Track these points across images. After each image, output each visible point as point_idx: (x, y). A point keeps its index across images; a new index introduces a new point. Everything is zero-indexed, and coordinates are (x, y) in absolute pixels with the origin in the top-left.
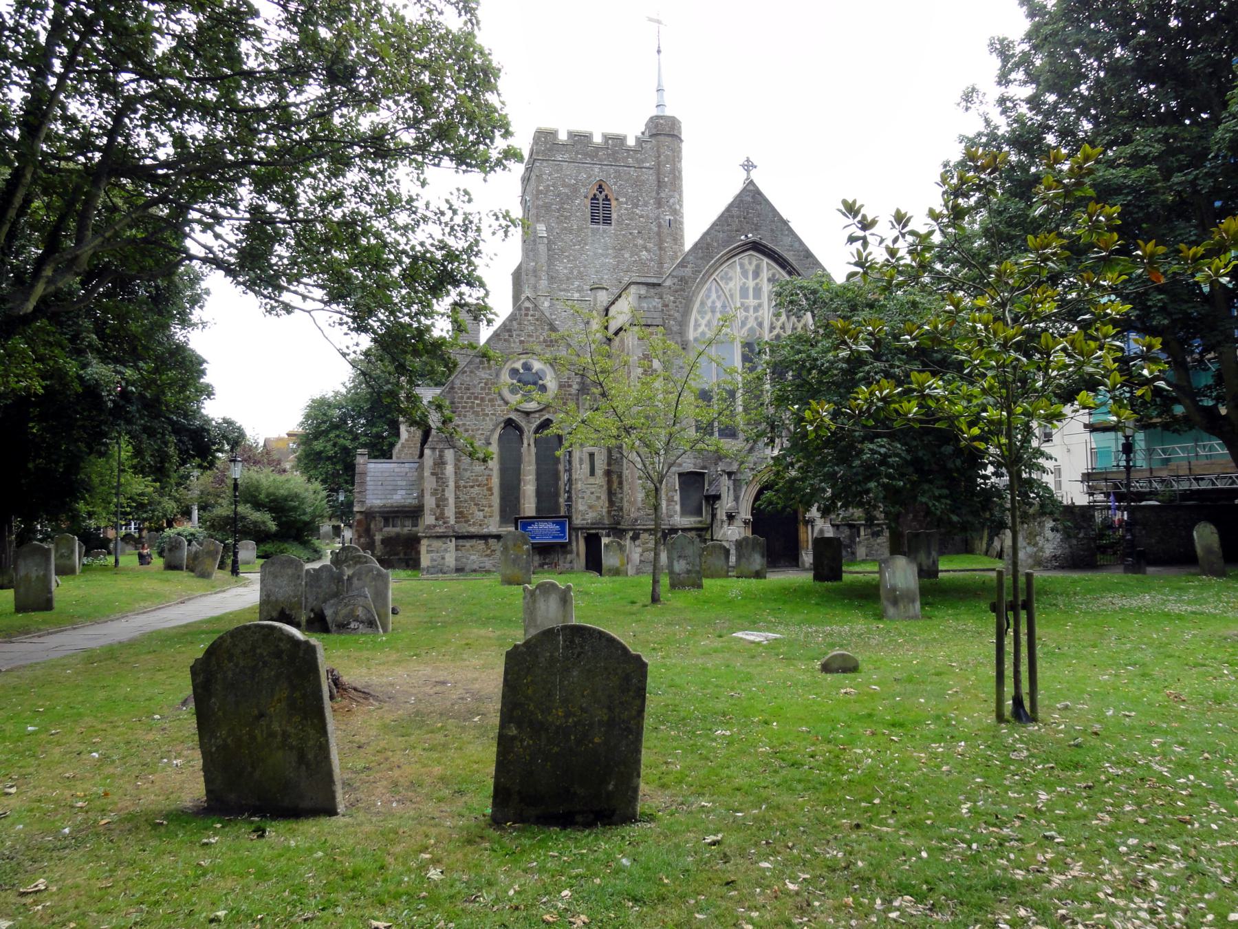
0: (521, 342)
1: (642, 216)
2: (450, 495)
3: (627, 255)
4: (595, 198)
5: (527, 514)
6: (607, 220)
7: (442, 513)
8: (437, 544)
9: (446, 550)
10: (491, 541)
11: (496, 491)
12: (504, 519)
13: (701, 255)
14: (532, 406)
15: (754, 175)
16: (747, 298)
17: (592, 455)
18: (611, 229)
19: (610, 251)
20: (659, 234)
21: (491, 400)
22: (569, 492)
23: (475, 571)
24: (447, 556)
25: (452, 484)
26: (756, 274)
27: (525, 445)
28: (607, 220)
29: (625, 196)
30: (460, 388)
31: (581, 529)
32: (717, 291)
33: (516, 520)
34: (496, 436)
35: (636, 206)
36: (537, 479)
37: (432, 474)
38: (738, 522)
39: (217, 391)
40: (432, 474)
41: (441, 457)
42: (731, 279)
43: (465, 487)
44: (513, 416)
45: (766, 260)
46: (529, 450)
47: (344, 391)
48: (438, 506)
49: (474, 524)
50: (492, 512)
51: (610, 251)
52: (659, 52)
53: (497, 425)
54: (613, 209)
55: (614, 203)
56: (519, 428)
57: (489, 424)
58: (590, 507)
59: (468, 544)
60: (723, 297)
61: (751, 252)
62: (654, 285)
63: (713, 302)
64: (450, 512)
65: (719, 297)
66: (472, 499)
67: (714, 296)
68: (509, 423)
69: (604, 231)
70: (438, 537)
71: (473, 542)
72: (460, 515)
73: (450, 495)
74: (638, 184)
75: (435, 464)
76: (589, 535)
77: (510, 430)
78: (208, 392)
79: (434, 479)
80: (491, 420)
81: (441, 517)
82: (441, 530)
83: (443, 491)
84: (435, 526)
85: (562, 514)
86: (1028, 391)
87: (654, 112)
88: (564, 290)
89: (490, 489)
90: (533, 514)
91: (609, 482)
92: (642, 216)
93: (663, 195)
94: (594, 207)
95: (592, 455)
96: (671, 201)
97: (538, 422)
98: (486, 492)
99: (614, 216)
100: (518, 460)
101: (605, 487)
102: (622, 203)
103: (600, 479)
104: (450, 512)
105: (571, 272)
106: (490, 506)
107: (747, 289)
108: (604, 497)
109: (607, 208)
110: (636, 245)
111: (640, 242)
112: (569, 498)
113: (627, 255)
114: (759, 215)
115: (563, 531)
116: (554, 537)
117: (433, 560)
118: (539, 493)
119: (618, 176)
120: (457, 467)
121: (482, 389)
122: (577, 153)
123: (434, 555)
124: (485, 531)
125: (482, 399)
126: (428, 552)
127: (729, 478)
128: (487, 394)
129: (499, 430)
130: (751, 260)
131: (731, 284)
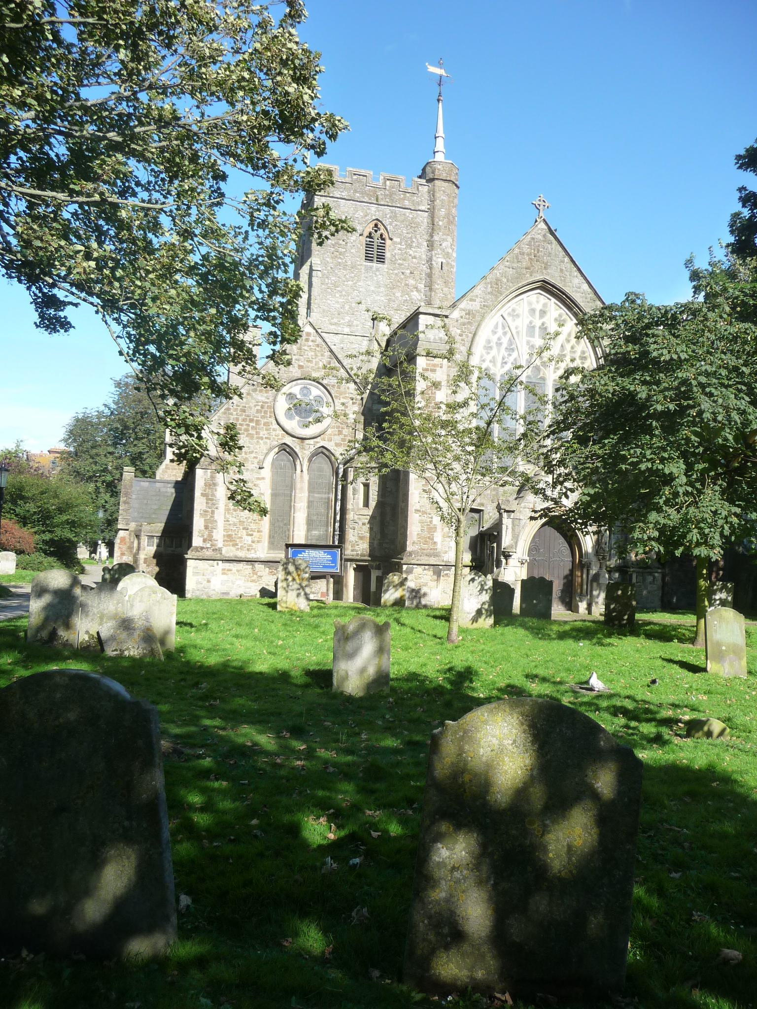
0: (300, 367)
1: (415, 257)
3: (398, 294)
4: (370, 236)
6: (381, 259)
12: (272, 545)
13: (489, 290)
16: (533, 336)
19: (382, 289)
20: (430, 276)
21: (266, 424)
23: (567, 692)
24: (213, 580)
28: (381, 259)
29: (400, 236)
30: (236, 410)
31: (351, 560)
32: (503, 327)
33: (288, 546)
35: (411, 247)
37: (202, 495)
40: (202, 495)
41: (213, 477)
44: (289, 440)
45: (553, 300)
46: (302, 477)
48: (206, 527)
49: (242, 548)
51: (382, 289)
53: (271, 449)
54: (387, 248)
55: (388, 242)
56: (292, 453)
57: (263, 447)
59: (234, 567)
60: (509, 334)
61: (539, 291)
63: (499, 339)
65: (505, 333)
67: (500, 331)
68: (285, 448)
69: (377, 270)
71: (241, 566)
72: (229, 539)
74: (413, 225)
77: (285, 456)
79: (204, 500)
80: (265, 443)
81: (208, 539)
82: (208, 553)
83: (213, 512)
84: (202, 548)
86: (131, 481)
88: (335, 324)
92: (415, 257)
93: (436, 238)
97: (312, 449)
99: (388, 255)
100: (291, 486)
102: (395, 243)
105: (343, 307)
107: (534, 327)
109: (382, 247)
113: (398, 294)
116: (324, 567)
117: (198, 583)
119: (394, 217)
121: (258, 411)
122: (355, 191)
124: (251, 555)
125: (258, 422)
127: (509, 517)
128: (263, 417)
129: (272, 454)
130: (539, 299)
131: (518, 322)
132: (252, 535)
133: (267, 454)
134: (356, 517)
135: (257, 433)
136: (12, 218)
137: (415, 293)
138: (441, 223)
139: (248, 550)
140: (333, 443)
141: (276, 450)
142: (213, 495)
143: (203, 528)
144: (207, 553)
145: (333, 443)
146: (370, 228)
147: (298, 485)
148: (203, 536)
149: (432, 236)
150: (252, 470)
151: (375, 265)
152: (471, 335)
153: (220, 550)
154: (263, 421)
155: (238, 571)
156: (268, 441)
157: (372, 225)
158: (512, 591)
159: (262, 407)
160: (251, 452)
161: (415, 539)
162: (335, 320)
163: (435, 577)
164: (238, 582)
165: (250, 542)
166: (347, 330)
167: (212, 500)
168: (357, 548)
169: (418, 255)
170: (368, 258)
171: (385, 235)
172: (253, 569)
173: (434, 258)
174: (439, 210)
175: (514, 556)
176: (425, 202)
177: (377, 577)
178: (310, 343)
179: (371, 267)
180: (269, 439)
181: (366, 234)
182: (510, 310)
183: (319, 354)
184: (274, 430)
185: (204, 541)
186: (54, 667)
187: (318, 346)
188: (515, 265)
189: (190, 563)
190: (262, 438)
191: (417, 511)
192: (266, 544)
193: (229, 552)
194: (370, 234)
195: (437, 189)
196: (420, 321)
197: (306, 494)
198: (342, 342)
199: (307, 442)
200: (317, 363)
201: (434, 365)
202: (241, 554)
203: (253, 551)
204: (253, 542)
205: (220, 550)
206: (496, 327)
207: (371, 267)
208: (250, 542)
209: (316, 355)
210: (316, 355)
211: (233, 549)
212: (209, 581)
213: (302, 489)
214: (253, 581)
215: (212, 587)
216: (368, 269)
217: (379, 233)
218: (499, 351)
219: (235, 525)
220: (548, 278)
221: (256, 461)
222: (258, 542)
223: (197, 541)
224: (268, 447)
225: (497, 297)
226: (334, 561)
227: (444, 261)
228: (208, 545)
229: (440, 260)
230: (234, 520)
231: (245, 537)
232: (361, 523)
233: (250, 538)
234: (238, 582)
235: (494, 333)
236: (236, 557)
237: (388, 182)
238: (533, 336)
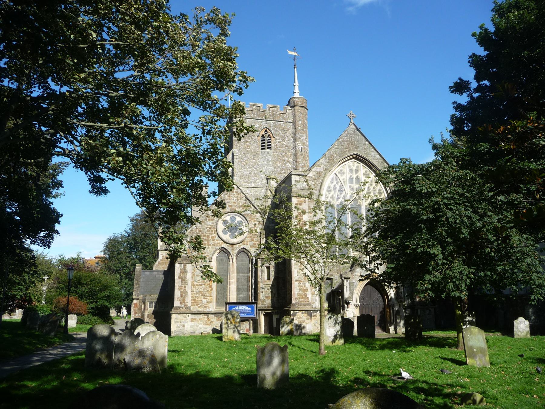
1: (287, 146)
2: (189, 289)
3: (279, 165)
4: (263, 136)
5: (231, 301)
6: (269, 148)
7: (184, 300)
9: (186, 321)
10: (210, 316)
12: (218, 304)
13: (328, 160)
14: (235, 241)
18: (271, 152)
20: (295, 155)
25: (190, 283)
26: (357, 171)
28: (269, 148)
29: (278, 135)
30: (196, 231)
31: (262, 310)
32: (336, 180)
33: (227, 304)
35: (284, 141)
36: (237, 281)
37: (179, 278)
38: (351, 306)
39: (61, 253)
41: (185, 268)
42: (344, 173)
43: (197, 285)
44: (225, 246)
45: (362, 164)
46: (233, 265)
47: (126, 234)
48: (182, 296)
50: (211, 299)
53: (216, 251)
54: (272, 142)
55: (273, 139)
56: (227, 253)
59: (197, 317)
62: (303, 176)
63: (335, 186)
65: (337, 183)
66: (201, 292)
67: (335, 182)
68: (223, 250)
71: (201, 316)
72: (194, 301)
74: (285, 130)
77: (223, 254)
78: (59, 222)
79: (180, 281)
81: (183, 302)
82: (183, 310)
83: (185, 287)
84: (180, 307)
88: (247, 182)
90: (235, 301)
93: (297, 135)
94: (263, 141)
96: (302, 139)
97: (238, 249)
99: (273, 145)
102: (277, 139)
104: (189, 300)
105: (251, 173)
107: (352, 179)
109: (269, 141)
110: (284, 160)
111: (286, 158)
113: (279, 165)
114: (358, 141)
115: (252, 311)
116: (247, 314)
119: (275, 126)
121: (208, 231)
122: (254, 114)
123: (179, 324)
124: (207, 310)
125: (208, 237)
126: (176, 322)
127: (347, 281)
129: (216, 253)
130: (354, 164)
131: (344, 176)
134: (263, 286)
135: (208, 242)
140: (249, 246)
141: (218, 251)
142: (185, 277)
145: (249, 246)
146: (262, 132)
147: (231, 270)
148: (180, 300)
149: (295, 135)
152: (319, 185)
153: (189, 308)
154: (211, 236)
155: (200, 319)
157: (264, 131)
159: (210, 228)
161: (297, 296)
162: (247, 180)
163: (309, 317)
164: (200, 326)
166: (253, 185)
167: (184, 280)
168: (265, 303)
169: (288, 144)
171: (271, 135)
172: (208, 318)
174: (298, 121)
175: (352, 303)
176: (291, 118)
178: (235, 193)
179: (264, 152)
181: (261, 135)
182: (339, 170)
184: (217, 240)
185: (181, 303)
187: (239, 194)
188: (340, 147)
189: (173, 317)
190: (211, 245)
191: (296, 281)
192: (215, 303)
193: (194, 309)
194: (263, 135)
195: (296, 111)
196: (292, 179)
198: (251, 191)
199: (235, 246)
201: (301, 201)
202: (201, 310)
204: (207, 302)
205: (189, 308)
206: (333, 179)
207: (264, 152)
209: (238, 200)
210: (238, 200)
212: (184, 326)
213: (233, 271)
214: (208, 324)
215: (186, 329)
216: (262, 153)
217: (267, 134)
218: (335, 192)
219: (197, 293)
222: (210, 302)
223: (177, 304)
224: (214, 249)
225: (332, 164)
226: (252, 311)
228: (183, 306)
229: (300, 147)
232: (266, 289)
235: (332, 183)
237: (271, 109)
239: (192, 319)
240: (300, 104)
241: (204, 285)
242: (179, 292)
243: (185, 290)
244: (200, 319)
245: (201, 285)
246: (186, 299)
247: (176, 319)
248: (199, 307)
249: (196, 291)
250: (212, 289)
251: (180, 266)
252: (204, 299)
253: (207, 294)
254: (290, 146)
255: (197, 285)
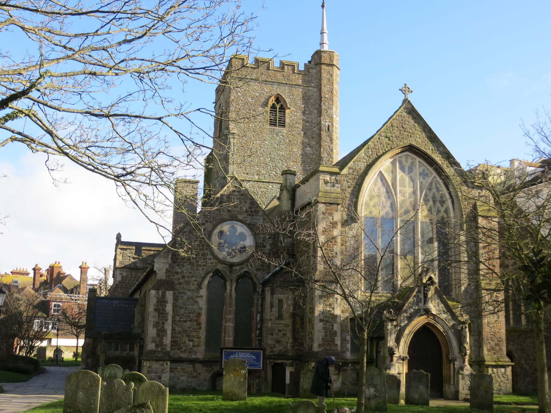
2: (168, 327)
8: (156, 365)
10: (198, 366)
11: (203, 326)
15: (410, 97)
17: (280, 301)
18: (284, 130)
22: (261, 329)
27: (228, 291)
34: (206, 282)
41: (164, 295)
44: (220, 267)
48: (158, 335)
49: (185, 351)
52: (323, 6)
53: (207, 274)
54: (286, 117)
58: (278, 342)
64: (168, 340)
66: (185, 331)
68: (217, 273)
70: (157, 360)
72: (174, 343)
73: (168, 327)
75: (157, 302)
76: (276, 364)
80: (203, 269)
81: (160, 344)
83: (163, 323)
85: (254, 346)
87: (318, 48)
89: (199, 324)
91: (294, 323)
95: (280, 301)
97: (239, 273)
98: (196, 327)
99: (287, 120)
101: (290, 327)
103: (288, 321)
106: (199, 338)
108: (289, 335)
112: (261, 334)
115: (258, 360)
118: (236, 330)
120: (175, 306)
128: (201, 250)
132: (193, 341)
133: (204, 278)
135: (197, 262)
136: (115, 160)
137: (308, 149)
138: (327, 96)
139: (190, 352)
141: (211, 274)
142: (165, 310)
143: (155, 336)
144: (159, 355)
148: (155, 342)
150: (193, 290)
151: (277, 128)
156: (205, 268)
158: (399, 382)
160: (192, 277)
163: (337, 372)
164: (182, 378)
165: (191, 347)
167: (163, 314)
168: (275, 349)
169: (310, 120)
170: (273, 123)
172: (194, 367)
173: (322, 122)
177: (291, 373)
180: (206, 266)
183: (243, 202)
184: (210, 259)
185: (157, 346)
186: (304, 400)
190: (200, 265)
194: (273, 104)
195: (323, 71)
196: (321, 177)
197: (234, 308)
199: (234, 268)
200: (241, 208)
202: (184, 356)
203: (193, 354)
204: (194, 346)
208: (191, 347)
211: (178, 351)
213: (230, 304)
214: (193, 377)
219: (179, 332)
220: (414, 143)
221: (196, 283)
222: (198, 346)
226: (258, 360)
227: (330, 124)
228: (159, 349)
229: (327, 124)
230: (179, 329)
231: (187, 342)
233: (191, 343)
234: (182, 378)
236: (180, 358)
238: (404, 187)
239: (171, 368)
240: (328, 62)
241: (190, 321)
242: (155, 329)
243: (164, 327)
244: (182, 369)
245: (185, 321)
246: (164, 341)
247: (150, 367)
248: (182, 352)
249: (177, 329)
250: (200, 328)
251: (158, 293)
252: (190, 341)
253: (194, 334)
254: (312, 122)
255: (180, 321)
